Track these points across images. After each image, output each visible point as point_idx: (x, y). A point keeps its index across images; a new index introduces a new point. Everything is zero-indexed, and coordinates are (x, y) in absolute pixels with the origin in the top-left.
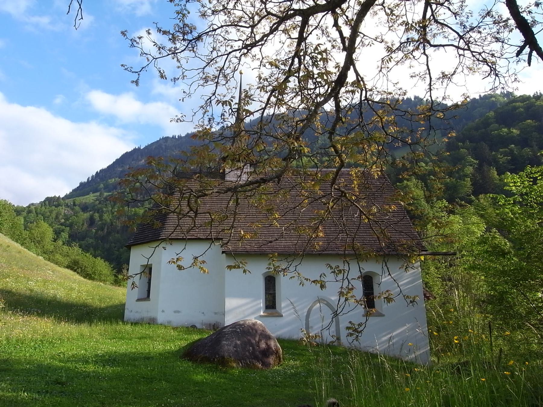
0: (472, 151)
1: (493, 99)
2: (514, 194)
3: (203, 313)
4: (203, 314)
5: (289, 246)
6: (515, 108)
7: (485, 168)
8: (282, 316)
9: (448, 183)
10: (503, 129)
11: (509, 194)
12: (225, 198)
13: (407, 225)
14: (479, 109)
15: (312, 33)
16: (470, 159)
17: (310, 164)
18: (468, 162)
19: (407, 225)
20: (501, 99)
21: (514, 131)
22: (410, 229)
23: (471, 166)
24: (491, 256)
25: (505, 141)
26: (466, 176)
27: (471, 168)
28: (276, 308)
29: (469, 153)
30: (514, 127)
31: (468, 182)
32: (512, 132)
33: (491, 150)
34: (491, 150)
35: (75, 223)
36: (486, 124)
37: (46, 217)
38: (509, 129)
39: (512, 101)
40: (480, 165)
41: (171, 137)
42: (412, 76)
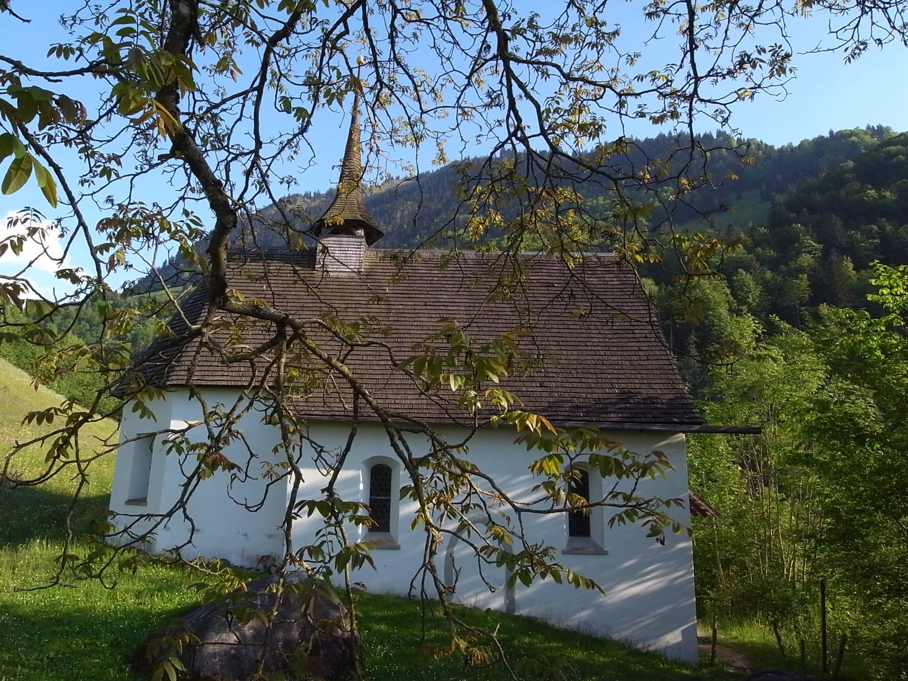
0: (812, 228)
1: (854, 138)
2: (888, 311)
3: (246, 535)
4: (245, 537)
5: (421, 406)
6: (891, 155)
7: (834, 257)
8: (397, 548)
9: (769, 282)
10: (869, 191)
11: (878, 310)
12: (309, 305)
13: (665, 367)
14: (829, 155)
15: (642, 95)
16: (810, 241)
17: (535, 244)
18: (805, 247)
19: (665, 367)
20: (868, 139)
21: (888, 194)
22: (670, 377)
23: (810, 253)
24: (836, 438)
25: (873, 212)
26: (801, 270)
27: (809, 256)
28: (388, 531)
29: (808, 232)
30: (887, 188)
31: (804, 281)
32: (885, 197)
33: (847, 227)
34: (847, 227)
35: (140, 336)
36: (838, 181)
37: (94, 325)
38: (878, 191)
39: (887, 142)
40: (826, 253)
41: (303, 194)
42: (650, 15)
